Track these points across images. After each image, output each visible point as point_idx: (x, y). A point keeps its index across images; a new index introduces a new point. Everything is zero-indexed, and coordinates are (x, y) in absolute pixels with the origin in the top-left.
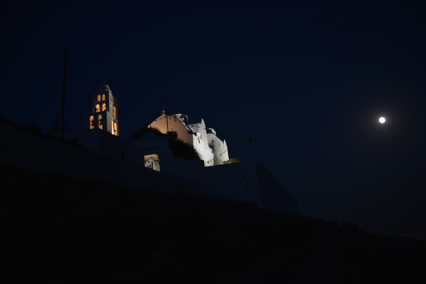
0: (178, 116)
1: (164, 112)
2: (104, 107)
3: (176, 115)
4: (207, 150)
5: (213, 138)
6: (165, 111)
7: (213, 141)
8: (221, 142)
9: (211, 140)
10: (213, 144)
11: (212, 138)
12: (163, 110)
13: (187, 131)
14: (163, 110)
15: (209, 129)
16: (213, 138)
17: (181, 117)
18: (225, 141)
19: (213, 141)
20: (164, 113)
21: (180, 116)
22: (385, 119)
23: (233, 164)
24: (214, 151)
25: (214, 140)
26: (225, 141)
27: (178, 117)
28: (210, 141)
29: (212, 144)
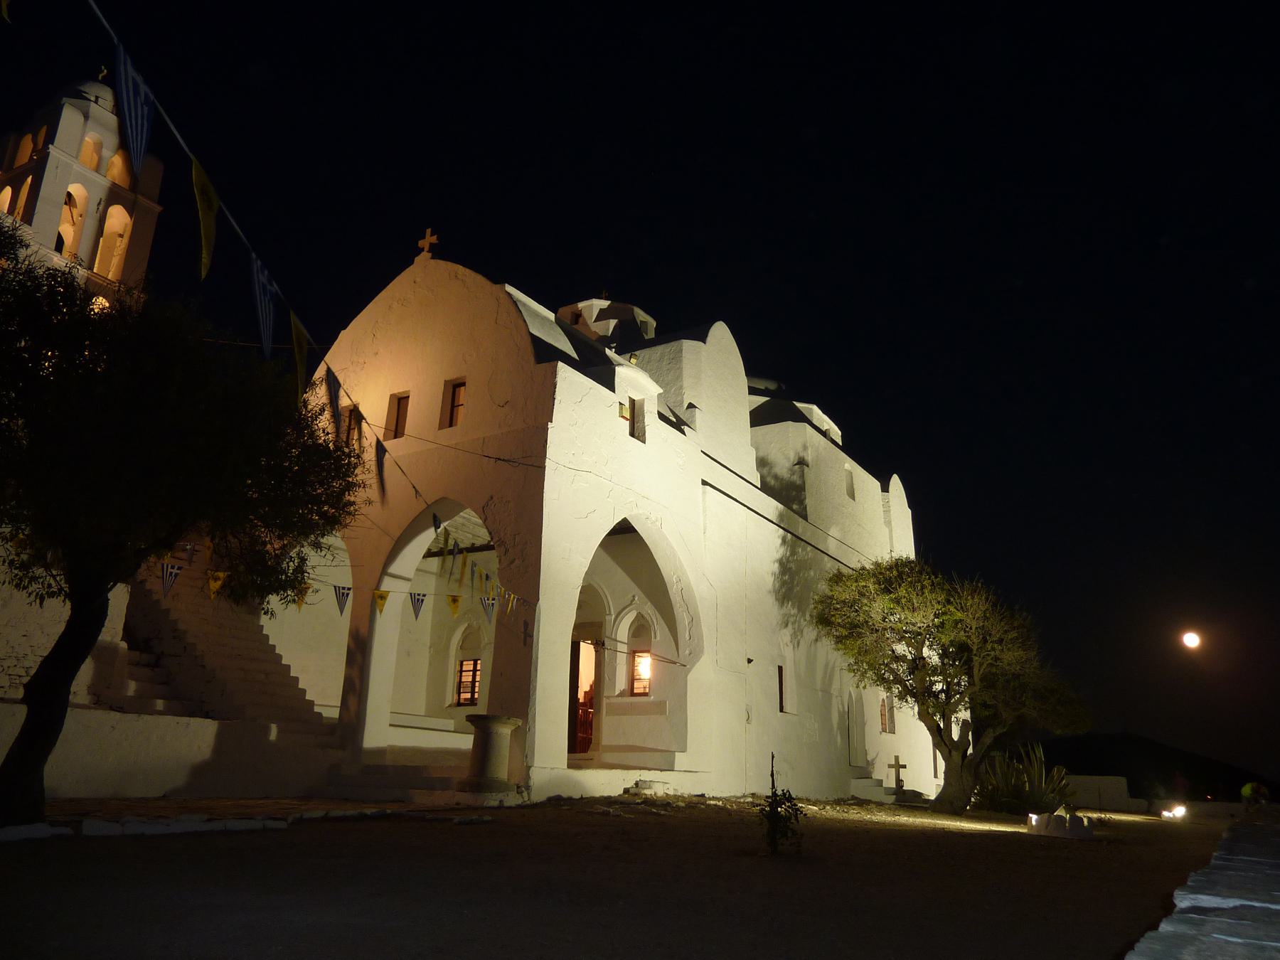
0: (591, 307)
1: (431, 244)
2: (322, 410)
3: (581, 305)
4: (559, 398)
5: (805, 448)
6: (434, 239)
7: (801, 462)
8: (867, 483)
9: (793, 458)
10: (802, 476)
11: (799, 447)
12: (429, 231)
13: (529, 339)
14: (429, 231)
15: (1054, 766)
16: (805, 448)
17: (603, 315)
18: (895, 481)
19: (801, 462)
20: (427, 249)
21: (601, 310)
22: (1185, 645)
23: (634, 305)
24: (507, 292)
25: (809, 458)
26: (895, 481)
27: (585, 314)
28: (788, 459)
29: (796, 478)
